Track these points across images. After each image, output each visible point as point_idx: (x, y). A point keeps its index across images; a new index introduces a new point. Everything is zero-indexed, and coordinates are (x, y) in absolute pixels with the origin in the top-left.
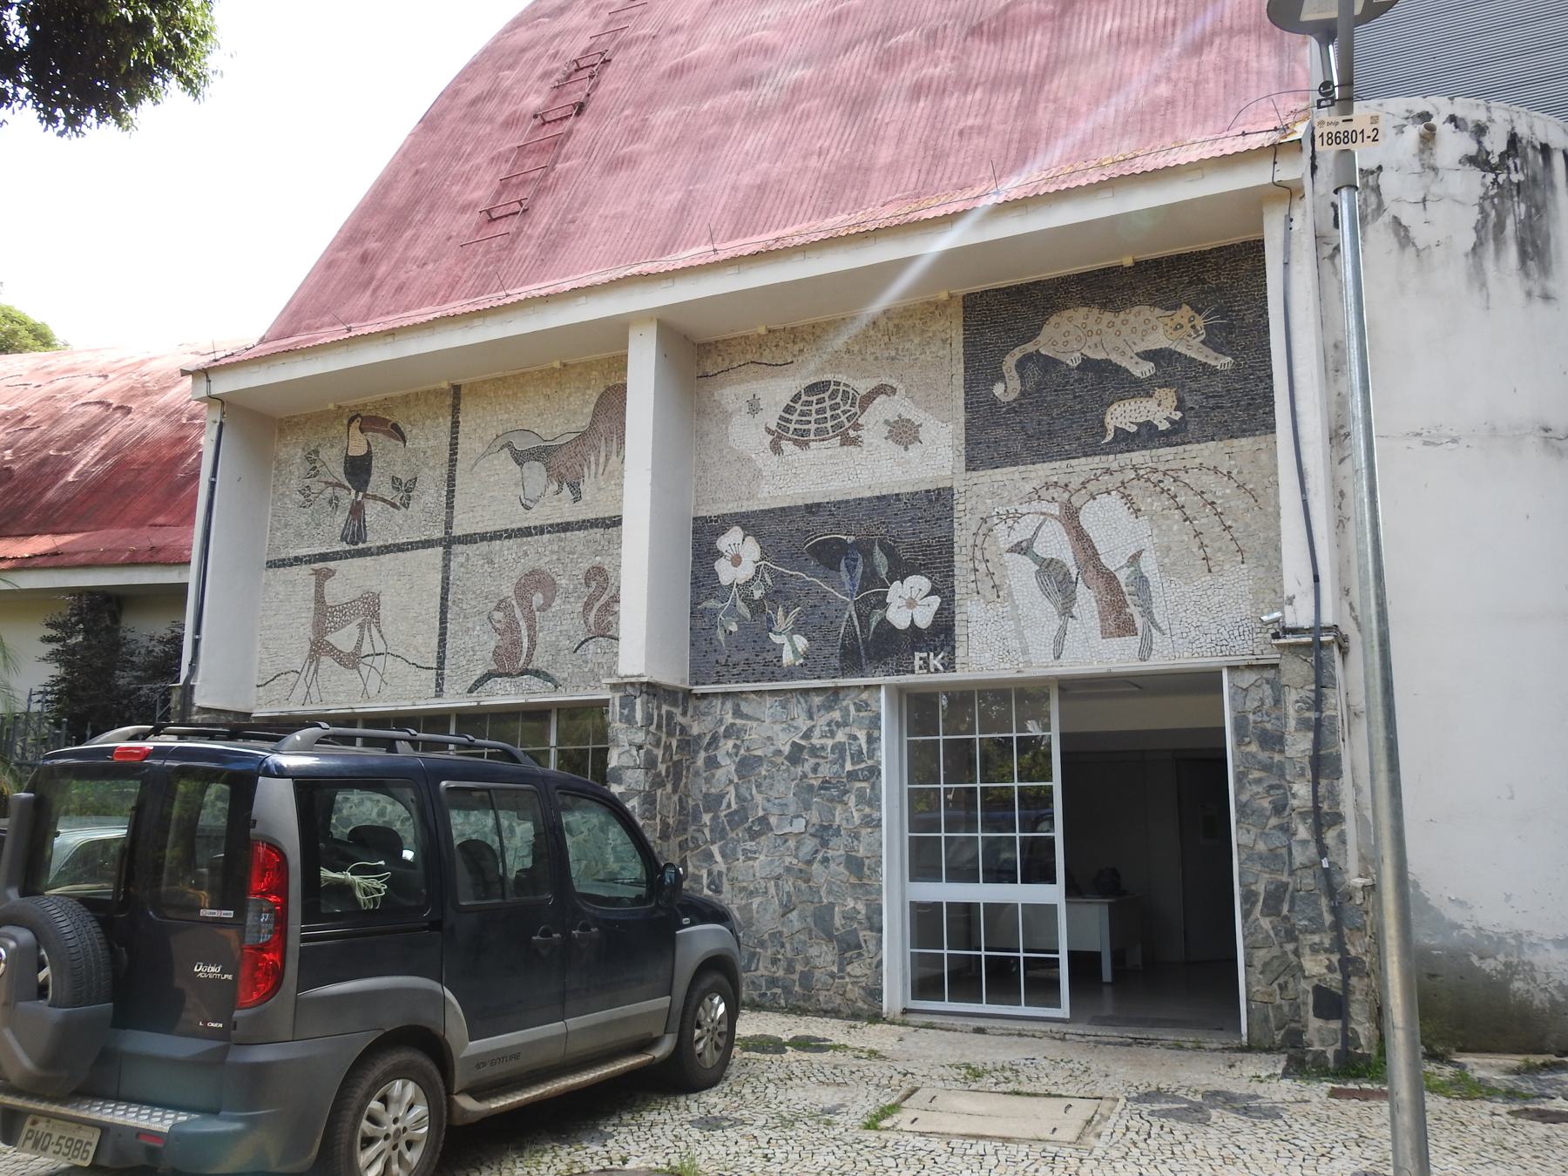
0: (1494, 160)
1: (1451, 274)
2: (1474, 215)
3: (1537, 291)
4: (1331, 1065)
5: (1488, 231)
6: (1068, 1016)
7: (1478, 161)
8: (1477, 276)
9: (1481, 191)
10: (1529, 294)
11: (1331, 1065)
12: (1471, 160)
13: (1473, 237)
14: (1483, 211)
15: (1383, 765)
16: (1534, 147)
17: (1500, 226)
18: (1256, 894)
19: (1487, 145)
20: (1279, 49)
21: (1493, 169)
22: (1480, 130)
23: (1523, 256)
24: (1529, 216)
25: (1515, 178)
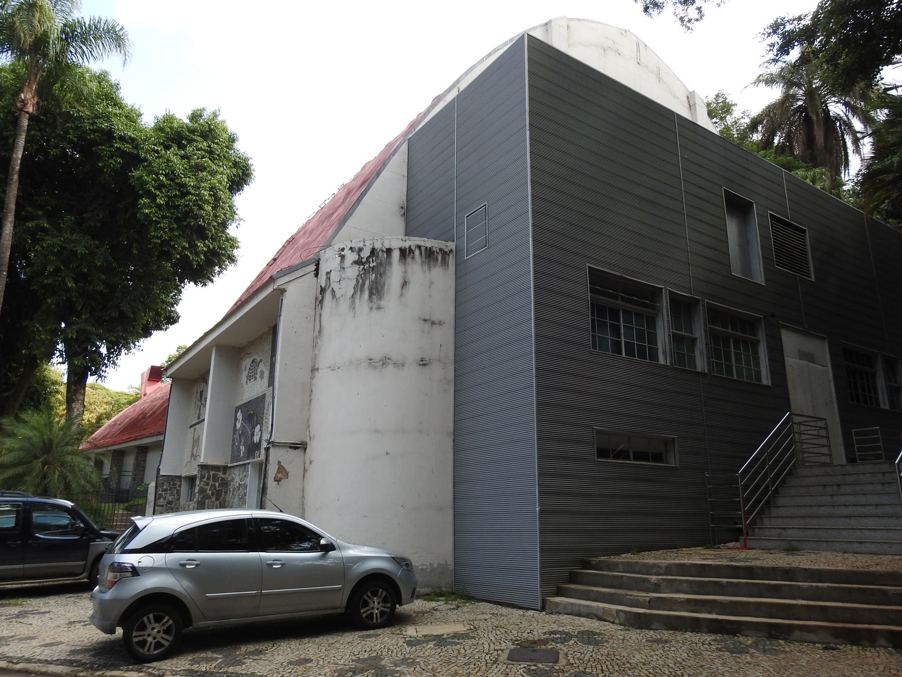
0: (364, 260)
1: (345, 306)
2: (354, 282)
3: (375, 306)
4: (184, 631)
5: (359, 288)
6: (162, 473)
7: (358, 262)
8: (353, 306)
9: (357, 273)
10: (371, 309)
11: (184, 631)
12: (355, 262)
13: (353, 291)
14: (357, 281)
15: (69, 581)
16: (383, 251)
17: (363, 285)
18: (42, 462)
19: (362, 255)
20: (92, 617)
21: (363, 264)
22: (360, 250)
23: (371, 294)
24: (376, 278)
25: (371, 265)
